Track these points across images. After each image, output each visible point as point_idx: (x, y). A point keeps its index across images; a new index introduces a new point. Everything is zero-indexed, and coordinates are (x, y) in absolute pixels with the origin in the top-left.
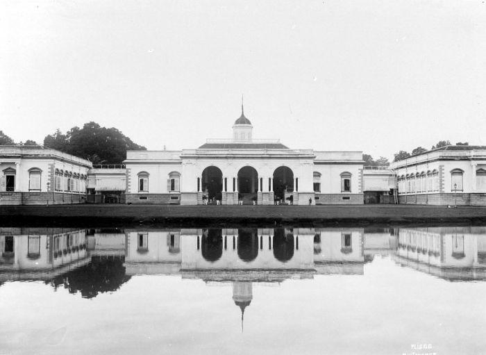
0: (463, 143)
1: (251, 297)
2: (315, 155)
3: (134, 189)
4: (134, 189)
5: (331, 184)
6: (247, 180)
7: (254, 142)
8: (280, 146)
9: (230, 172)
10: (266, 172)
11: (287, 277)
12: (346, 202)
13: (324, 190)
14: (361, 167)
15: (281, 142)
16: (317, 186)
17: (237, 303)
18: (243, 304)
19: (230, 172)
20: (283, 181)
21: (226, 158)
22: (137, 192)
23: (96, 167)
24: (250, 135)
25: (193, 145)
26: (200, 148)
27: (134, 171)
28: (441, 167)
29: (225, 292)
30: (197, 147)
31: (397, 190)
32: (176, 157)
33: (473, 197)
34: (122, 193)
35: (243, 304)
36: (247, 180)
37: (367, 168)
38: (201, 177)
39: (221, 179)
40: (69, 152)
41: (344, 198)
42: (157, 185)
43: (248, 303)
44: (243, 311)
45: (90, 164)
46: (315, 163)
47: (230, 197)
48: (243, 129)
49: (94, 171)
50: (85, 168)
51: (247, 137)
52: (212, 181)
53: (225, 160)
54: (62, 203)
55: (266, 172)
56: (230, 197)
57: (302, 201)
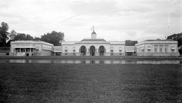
0: (34, 35)
2: (110, 42)
6: (92, 48)
7: (97, 39)
8: (103, 40)
9: (88, 47)
10: (97, 47)
13: (114, 52)
16: (112, 51)
19: (88, 47)
20: (102, 50)
21: (87, 43)
23: (54, 46)
24: (96, 37)
25: (79, 40)
26: (82, 41)
28: (144, 46)
31: (136, 52)
33: (153, 54)
34: (133, 54)
36: (92, 48)
37: (126, 46)
38: (89, 49)
39: (95, 49)
40: (50, 43)
42: (70, 51)
43: (92, 33)
45: (53, 45)
47: (88, 54)
48: (94, 35)
50: (51, 46)
52: (83, 50)
53: (96, 44)
55: (97, 47)
56: (88, 54)
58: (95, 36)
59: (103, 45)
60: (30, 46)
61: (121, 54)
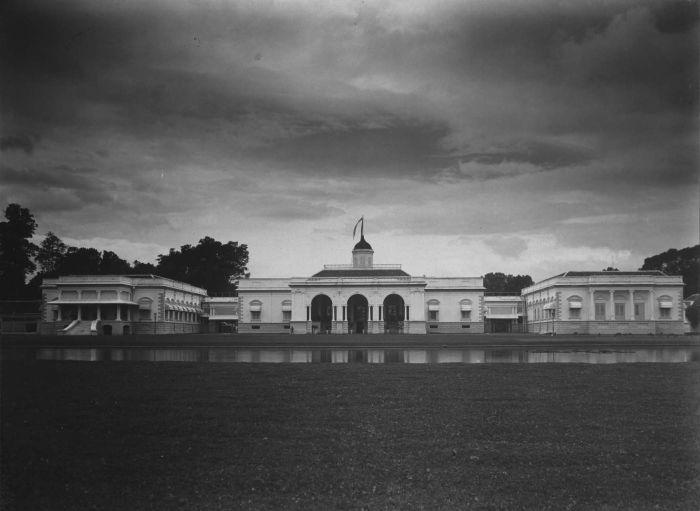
1: (354, 253)
3: (247, 319)
4: (247, 319)
5: (449, 312)
6: (358, 305)
8: (399, 273)
9: (340, 300)
10: (376, 300)
11: (309, 279)
12: (434, 330)
14: (482, 294)
15: (403, 269)
16: (433, 314)
17: (368, 246)
18: (363, 246)
19: (340, 300)
22: (249, 321)
23: (211, 295)
26: (315, 276)
27: (247, 300)
28: (557, 293)
29: (381, 259)
30: (310, 276)
32: (285, 286)
35: (363, 246)
36: (358, 305)
41: (464, 327)
42: (272, 313)
43: (357, 247)
44: (362, 237)
46: (426, 290)
49: (208, 300)
51: (367, 263)
52: (321, 309)
54: (173, 332)
55: (376, 300)
57: (414, 330)
58: (369, 255)
59: (399, 292)
60: (116, 299)
61: (468, 327)
